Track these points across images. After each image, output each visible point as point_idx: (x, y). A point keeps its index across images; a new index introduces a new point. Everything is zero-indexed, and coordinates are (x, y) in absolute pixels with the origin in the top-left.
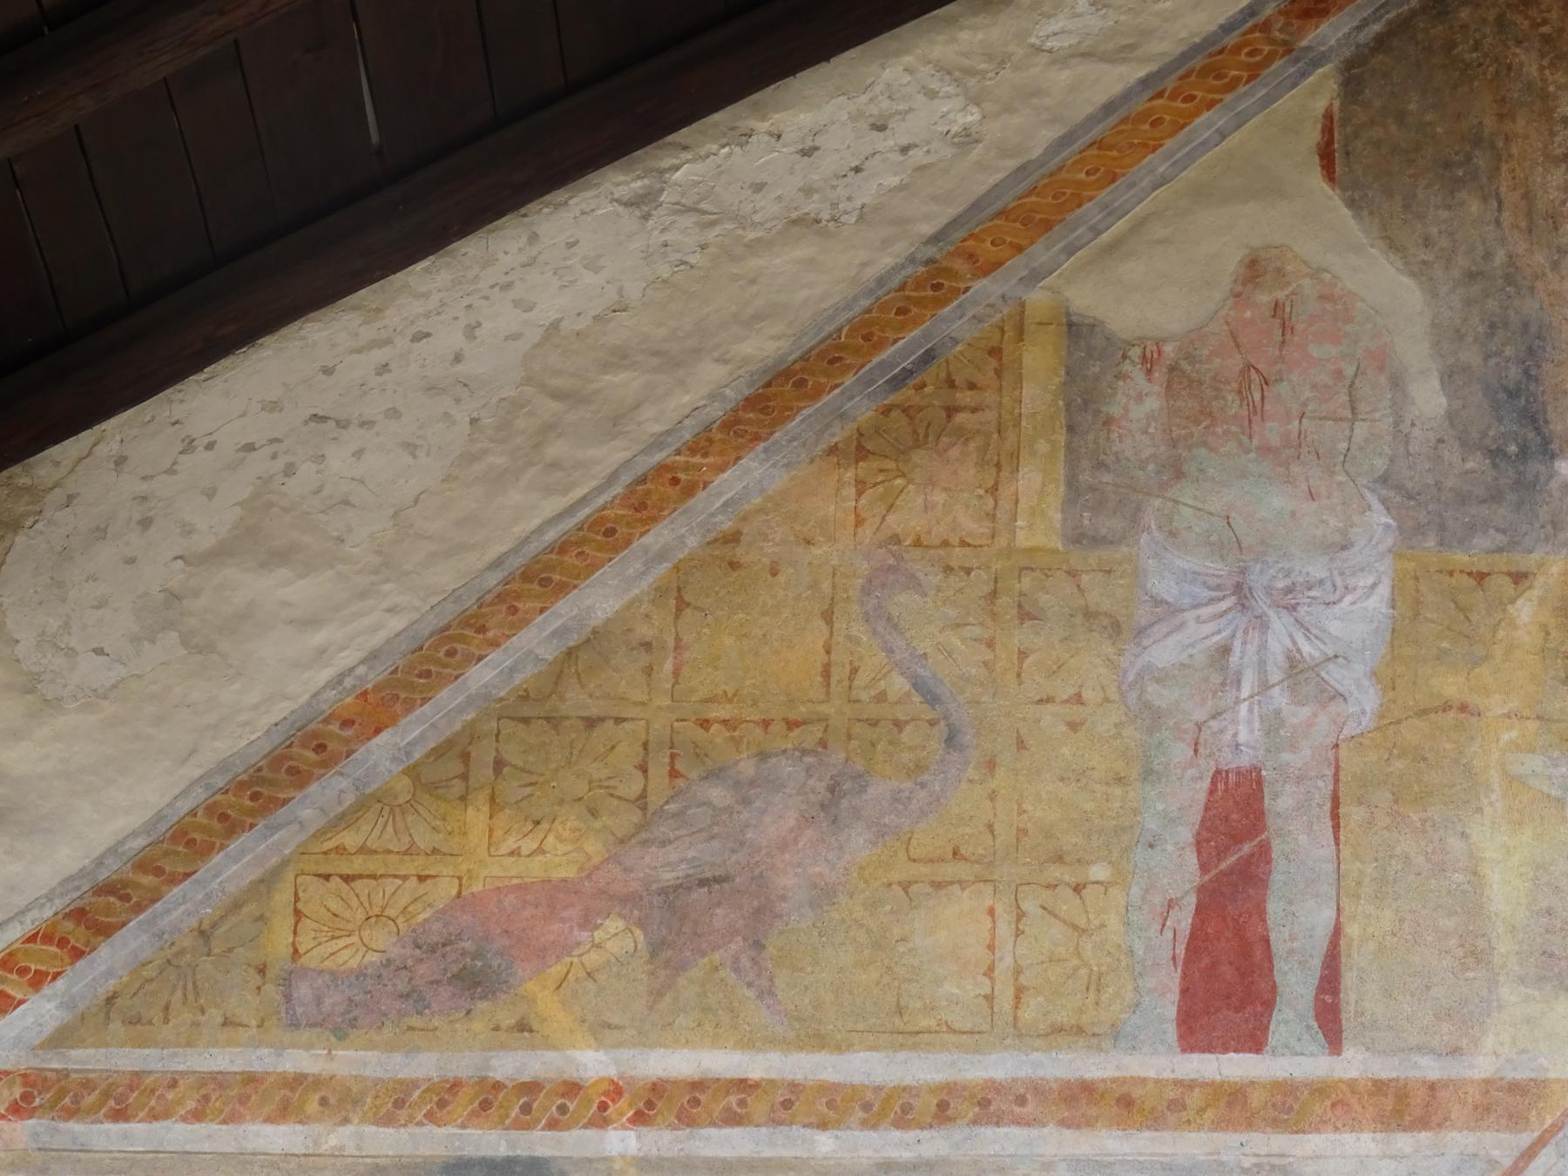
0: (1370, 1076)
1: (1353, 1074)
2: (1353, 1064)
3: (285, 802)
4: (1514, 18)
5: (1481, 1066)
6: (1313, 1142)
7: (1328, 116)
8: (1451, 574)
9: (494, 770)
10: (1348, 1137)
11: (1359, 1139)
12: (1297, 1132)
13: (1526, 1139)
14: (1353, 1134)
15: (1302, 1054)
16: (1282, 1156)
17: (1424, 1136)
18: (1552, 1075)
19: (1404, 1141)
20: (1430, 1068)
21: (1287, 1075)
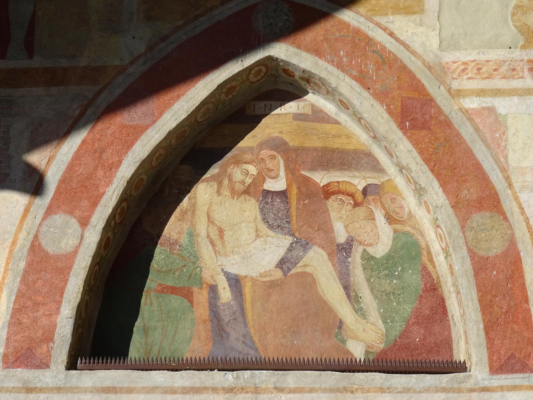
0: (43, 66)
1: (37, 66)
2: (37, 62)
3: (104, 193)
4: (448, 277)
5: (84, 62)
6: (22, 91)
7: (87, 301)
8: (376, 388)
9: (367, 191)
10: (34, 89)
11: (38, 89)
12: (16, 88)
13: (98, 88)
14: (36, 88)
15: (19, 59)
16: (10, 96)
17: (61, 88)
18: (108, 64)
19: (54, 90)
20: (64, 63)
21: (13, 67)
